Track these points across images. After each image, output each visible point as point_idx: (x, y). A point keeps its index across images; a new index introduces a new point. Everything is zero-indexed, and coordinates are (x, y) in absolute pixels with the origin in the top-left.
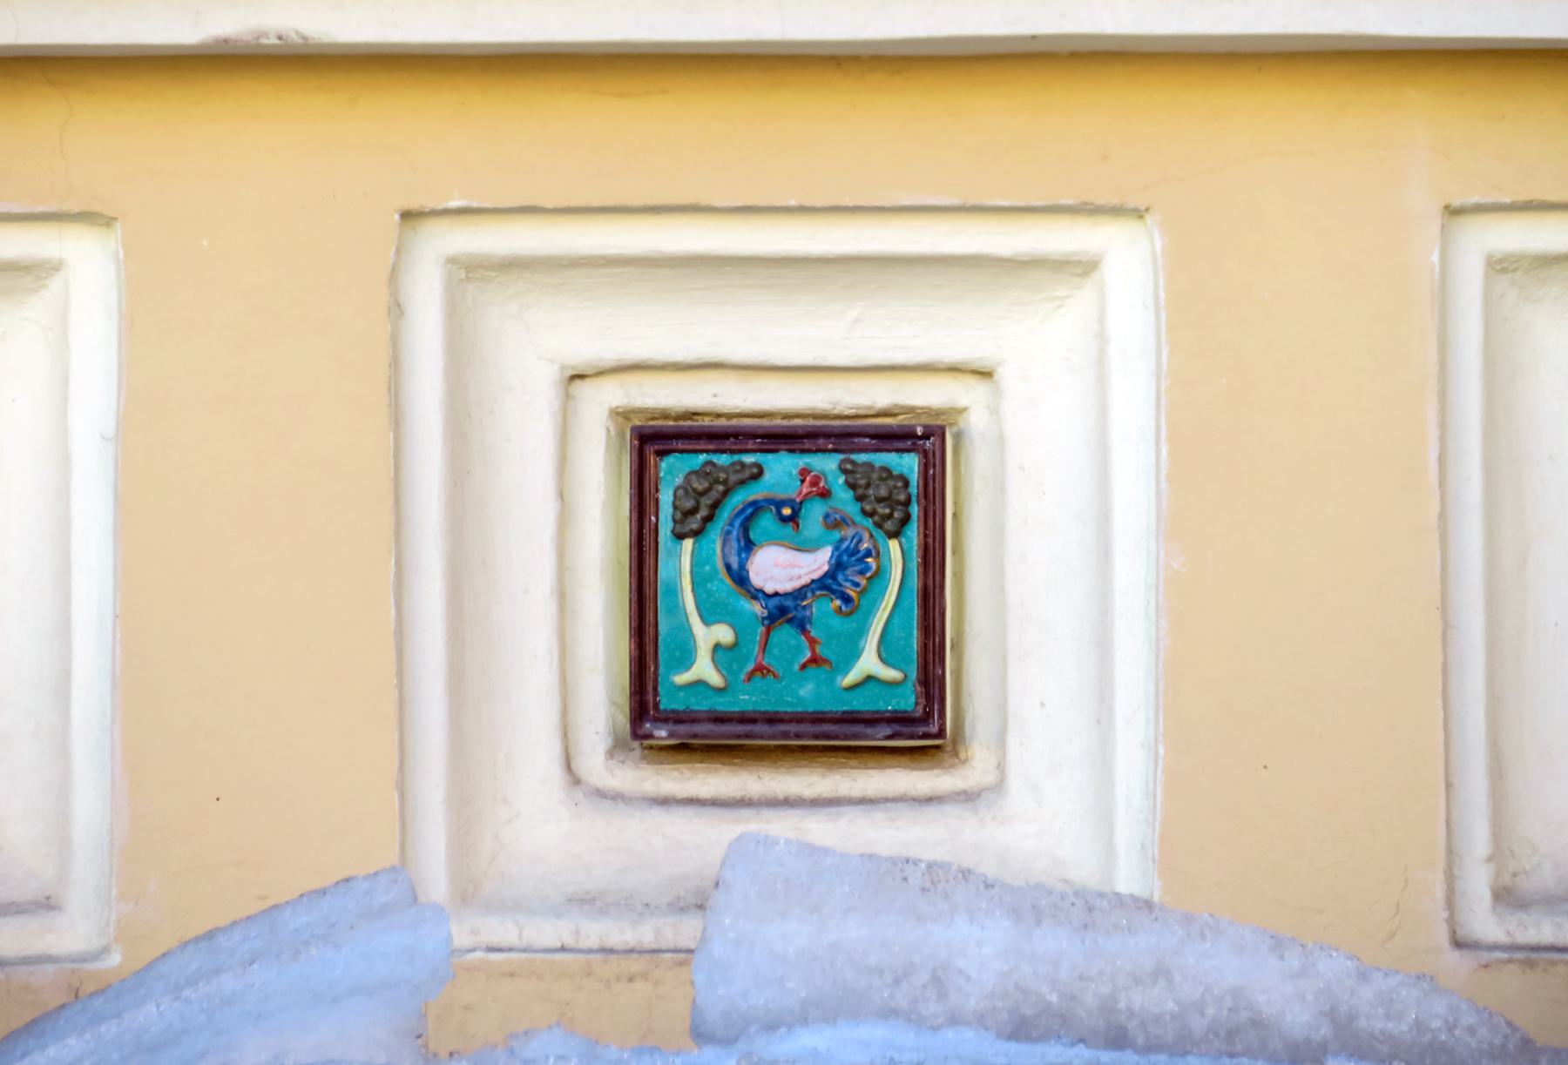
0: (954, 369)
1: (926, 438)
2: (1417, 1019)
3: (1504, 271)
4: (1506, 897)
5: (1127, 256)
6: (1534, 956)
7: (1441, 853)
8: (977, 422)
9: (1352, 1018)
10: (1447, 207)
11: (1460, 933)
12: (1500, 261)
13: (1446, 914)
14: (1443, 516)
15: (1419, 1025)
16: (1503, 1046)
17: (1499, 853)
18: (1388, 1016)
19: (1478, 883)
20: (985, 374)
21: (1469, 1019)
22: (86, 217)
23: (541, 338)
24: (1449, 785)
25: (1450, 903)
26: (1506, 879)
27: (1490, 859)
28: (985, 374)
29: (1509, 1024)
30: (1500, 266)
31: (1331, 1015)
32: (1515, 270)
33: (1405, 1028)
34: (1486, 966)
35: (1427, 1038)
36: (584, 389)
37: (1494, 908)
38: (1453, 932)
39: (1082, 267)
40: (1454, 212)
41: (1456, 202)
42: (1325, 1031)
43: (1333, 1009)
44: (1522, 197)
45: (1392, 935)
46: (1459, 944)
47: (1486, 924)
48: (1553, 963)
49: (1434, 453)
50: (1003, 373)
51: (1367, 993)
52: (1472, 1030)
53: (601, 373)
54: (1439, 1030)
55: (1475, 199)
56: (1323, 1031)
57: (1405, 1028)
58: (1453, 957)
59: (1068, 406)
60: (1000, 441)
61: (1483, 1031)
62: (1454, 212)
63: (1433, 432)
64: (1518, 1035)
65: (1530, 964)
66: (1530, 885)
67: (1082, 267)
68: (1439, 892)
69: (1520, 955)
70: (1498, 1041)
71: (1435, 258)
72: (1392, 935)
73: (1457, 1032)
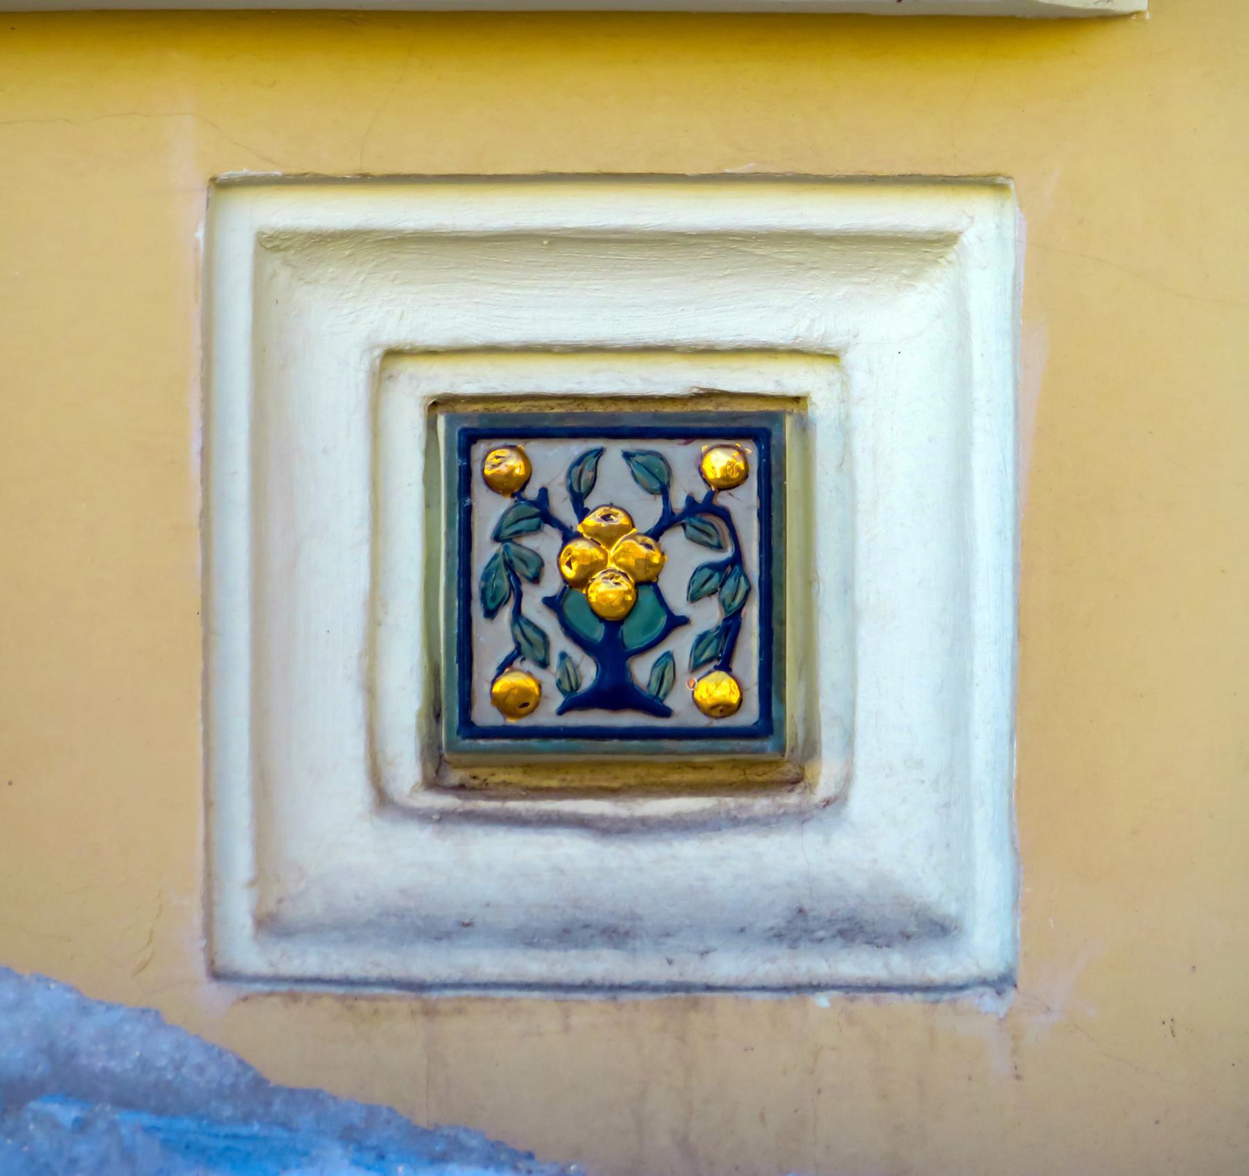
0: (794, 352)
1: (762, 430)
2: (141, 1056)
3: (276, 249)
4: (269, 925)
5: (986, 231)
6: (298, 988)
7: (199, 879)
8: (822, 408)
9: (72, 1055)
10: (213, 180)
11: (220, 963)
12: (272, 238)
13: (203, 943)
14: (206, 514)
15: (144, 1064)
16: (234, 1086)
17: (259, 880)
18: (110, 1054)
19: (239, 908)
20: (829, 355)
21: (197, 1058)
22: (990, 183)
23: (346, 321)
24: (208, 805)
25: (209, 930)
26: (271, 906)
27: (252, 883)
28: (829, 355)
29: (241, 1062)
30: (272, 244)
31: (50, 1051)
32: (287, 249)
33: (128, 1065)
34: (245, 999)
35: (152, 1077)
36: (408, 367)
37: (255, 938)
38: (211, 963)
39: (936, 244)
40: (221, 185)
41: (224, 174)
42: (41, 1068)
43: (52, 1045)
44: (295, 170)
45: (144, 966)
46: (218, 975)
47: (248, 954)
48: (317, 996)
49: (196, 446)
50: (850, 358)
51: (88, 1029)
52: (201, 1070)
53: (431, 352)
54: (165, 1068)
55: (245, 171)
56: (40, 1069)
57: (128, 1065)
58: (212, 990)
59: (927, 393)
60: (845, 430)
61: (213, 1071)
62: (221, 185)
63: (196, 423)
64: (250, 1074)
65: (294, 997)
66: (293, 913)
67: (936, 244)
68: (197, 920)
69: (283, 988)
70: (228, 1080)
71: (200, 234)
72: (144, 966)
73: (185, 1070)
